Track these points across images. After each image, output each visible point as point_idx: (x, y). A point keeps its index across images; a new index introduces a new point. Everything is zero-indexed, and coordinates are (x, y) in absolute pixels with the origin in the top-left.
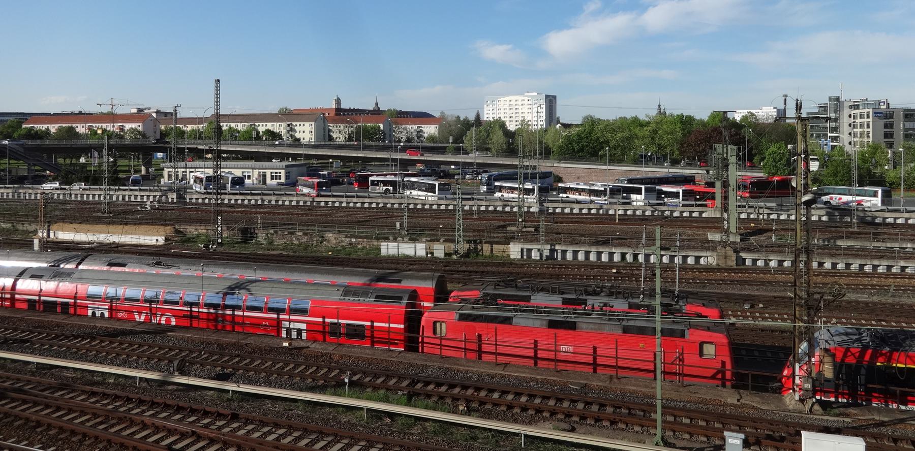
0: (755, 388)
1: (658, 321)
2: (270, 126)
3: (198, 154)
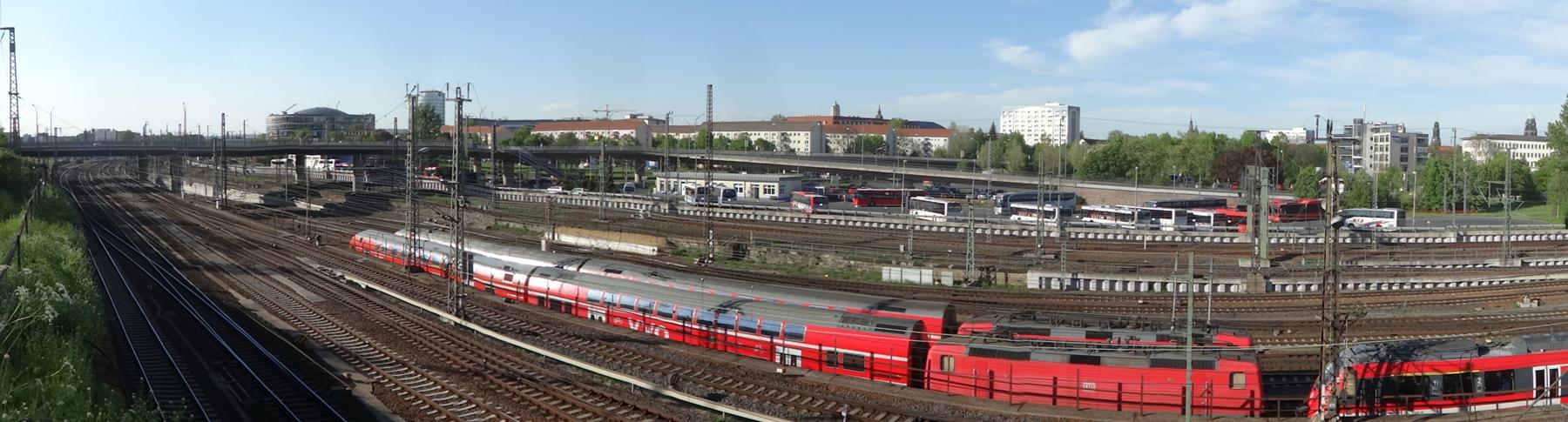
0: (1284, 415)
1: (1189, 352)
2: (763, 135)
3: (690, 164)
